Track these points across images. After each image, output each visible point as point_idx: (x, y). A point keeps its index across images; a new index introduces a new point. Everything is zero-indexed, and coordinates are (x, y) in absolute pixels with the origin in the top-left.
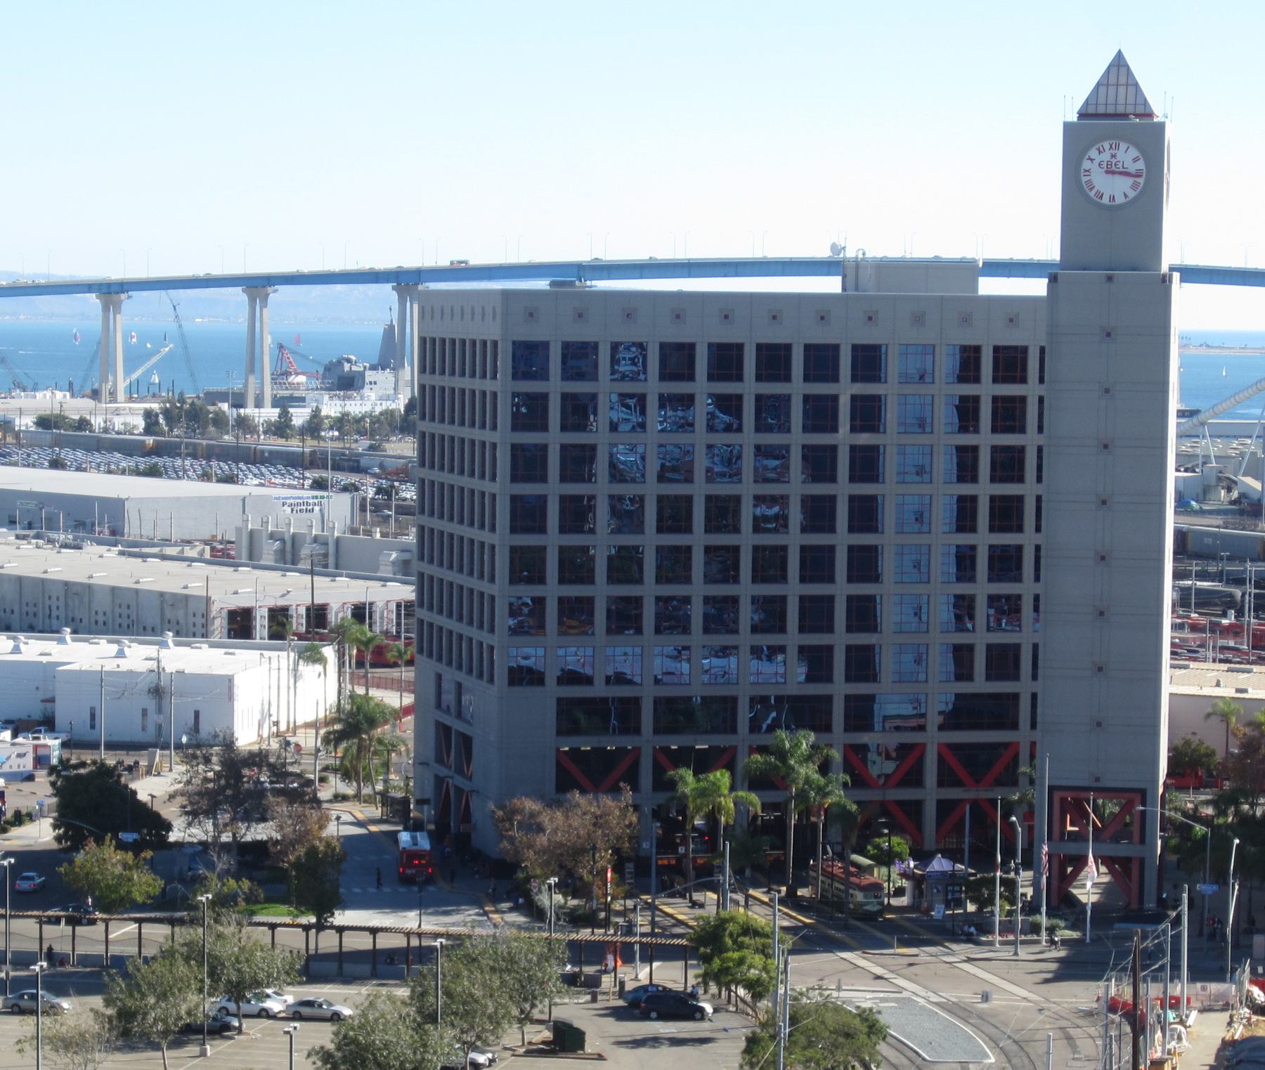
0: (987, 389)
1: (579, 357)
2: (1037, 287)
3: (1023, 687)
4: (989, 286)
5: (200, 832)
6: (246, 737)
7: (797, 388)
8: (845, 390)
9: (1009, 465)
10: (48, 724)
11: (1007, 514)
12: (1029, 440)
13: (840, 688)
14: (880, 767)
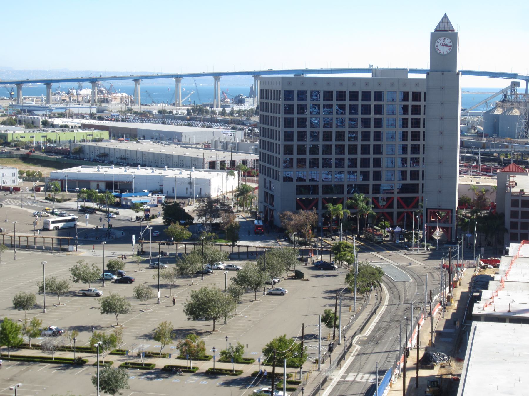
0: (410, 103)
1: (302, 95)
2: (424, 76)
3: (420, 182)
4: (411, 76)
5: (202, 220)
6: (214, 195)
7: (360, 103)
10: (161, 192)
11: (415, 149)
13: (371, 182)
14: (382, 203)
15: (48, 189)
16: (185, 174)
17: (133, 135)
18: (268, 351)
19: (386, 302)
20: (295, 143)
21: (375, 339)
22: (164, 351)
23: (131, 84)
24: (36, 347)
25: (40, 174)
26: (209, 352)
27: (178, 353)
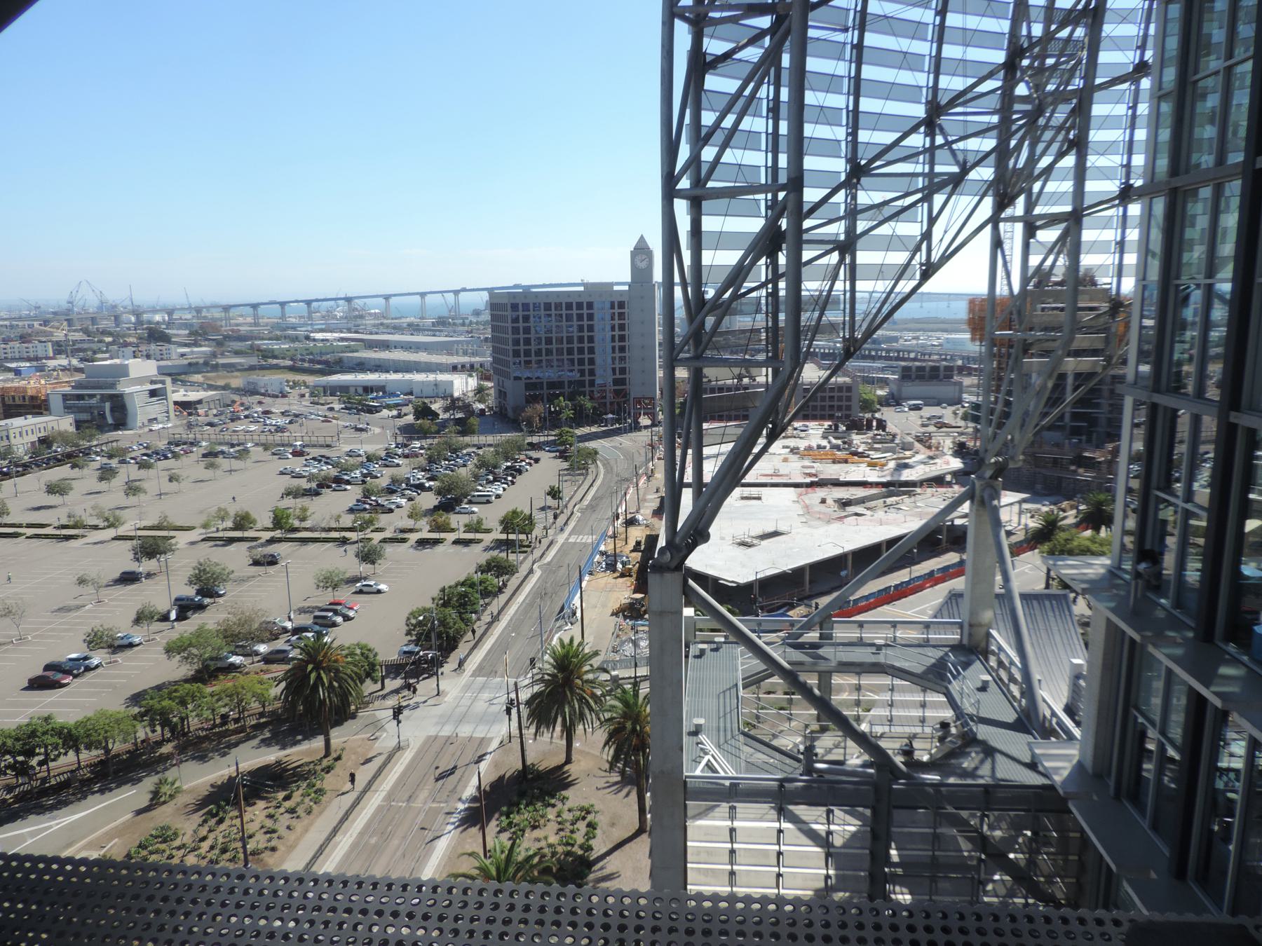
0: (617, 311)
1: (526, 307)
2: (626, 288)
3: (627, 376)
4: (616, 288)
5: (446, 416)
6: (456, 394)
7: (575, 312)
8: (585, 311)
9: (622, 338)
10: (411, 394)
11: (622, 349)
12: (626, 333)
13: (587, 378)
14: (597, 395)
15: (312, 394)
16: (431, 377)
17: (386, 346)
18: (502, 522)
19: (601, 476)
20: (522, 347)
21: (592, 507)
22: (417, 527)
23: (382, 301)
24: (306, 529)
25: (304, 382)
26: (453, 526)
27: (428, 528)
